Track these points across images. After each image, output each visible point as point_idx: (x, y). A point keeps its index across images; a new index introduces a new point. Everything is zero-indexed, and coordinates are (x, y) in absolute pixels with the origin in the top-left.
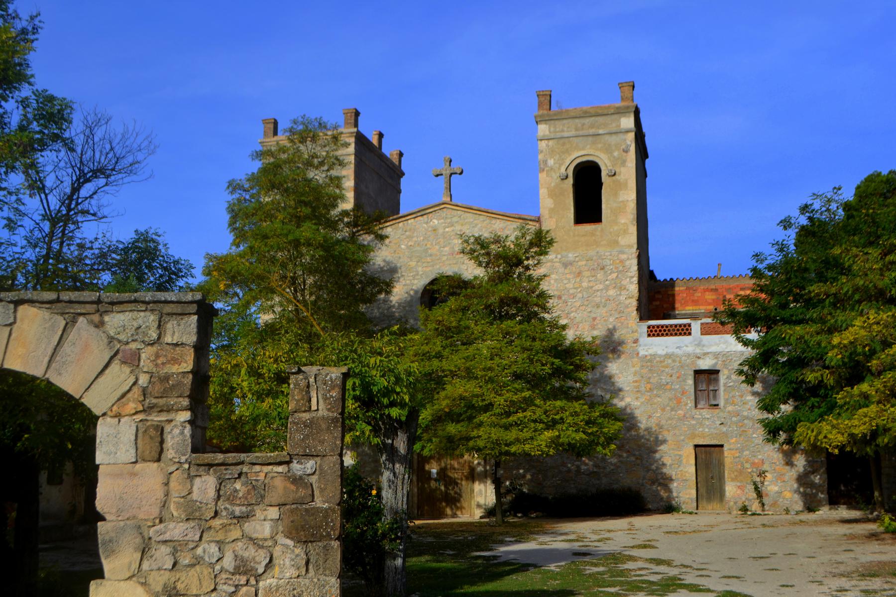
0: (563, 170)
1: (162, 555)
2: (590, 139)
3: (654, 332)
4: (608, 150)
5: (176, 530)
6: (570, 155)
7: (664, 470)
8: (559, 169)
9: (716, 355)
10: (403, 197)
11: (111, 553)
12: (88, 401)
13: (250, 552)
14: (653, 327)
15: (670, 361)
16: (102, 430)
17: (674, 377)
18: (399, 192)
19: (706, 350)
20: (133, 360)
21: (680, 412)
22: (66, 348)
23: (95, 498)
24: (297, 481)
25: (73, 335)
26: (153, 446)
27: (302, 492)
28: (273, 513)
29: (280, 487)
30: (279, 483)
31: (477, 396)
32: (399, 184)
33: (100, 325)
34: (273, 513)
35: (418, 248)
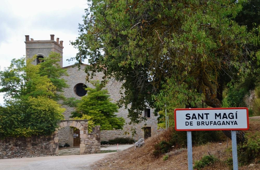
1: (86, 142)
5: (87, 139)
7: (223, 91)
10: (63, 54)
11: (82, 141)
12: (79, 129)
13: (93, 141)
16: (80, 131)
18: (62, 53)
20: (83, 125)
22: (77, 124)
23: (151, 133)
24: (97, 135)
25: (78, 123)
26: (85, 133)
27: (97, 136)
28: (95, 138)
29: (95, 136)
30: (95, 136)
31: (13, 101)
32: (62, 51)
33: (80, 122)
34: (95, 138)
35: (73, 75)
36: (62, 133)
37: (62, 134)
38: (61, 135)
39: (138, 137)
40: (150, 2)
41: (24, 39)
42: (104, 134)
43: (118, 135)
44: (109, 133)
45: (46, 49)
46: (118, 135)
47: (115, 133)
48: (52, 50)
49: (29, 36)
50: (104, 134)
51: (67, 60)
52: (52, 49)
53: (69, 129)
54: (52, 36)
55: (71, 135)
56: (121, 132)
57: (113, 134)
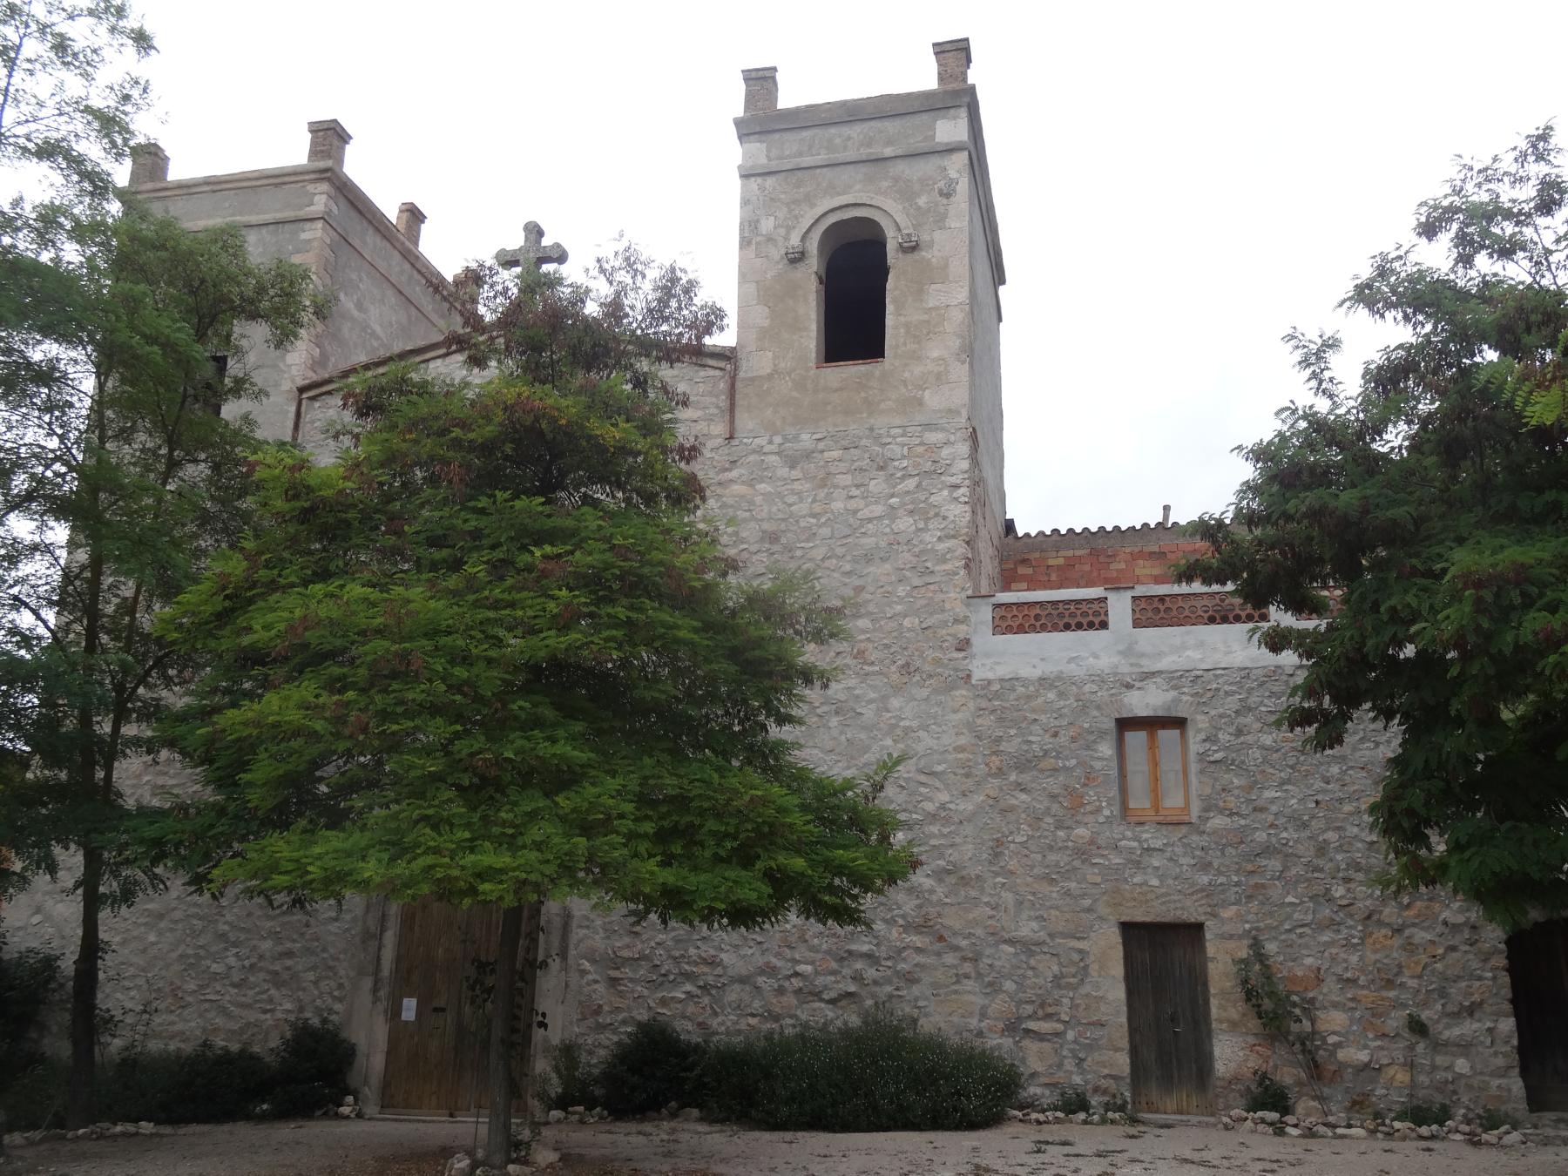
0: (795, 240)
2: (863, 169)
3: (1013, 620)
4: (907, 194)
6: (813, 206)
8: (787, 238)
9: (1175, 679)
14: (1008, 605)
15: (1051, 695)
17: (1063, 739)
19: (1149, 665)
21: (1081, 831)
36: (289, 963)
37: (286, 976)
38: (278, 985)
39: (1057, 1034)
40: (545, 1156)
41: (16, 195)
42: (688, 987)
43: (832, 1002)
44: (743, 980)
45: (264, 230)
46: (832, 1002)
47: (797, 983)
48: (304, 236)
49: (775, 69)
50: (688, 987)
51: (954, 54)
52: (308, 225)
53: (354, 919)
54: (329, 137)
55: (368, 983)
56: (871, 973)
57: (781, 991)
